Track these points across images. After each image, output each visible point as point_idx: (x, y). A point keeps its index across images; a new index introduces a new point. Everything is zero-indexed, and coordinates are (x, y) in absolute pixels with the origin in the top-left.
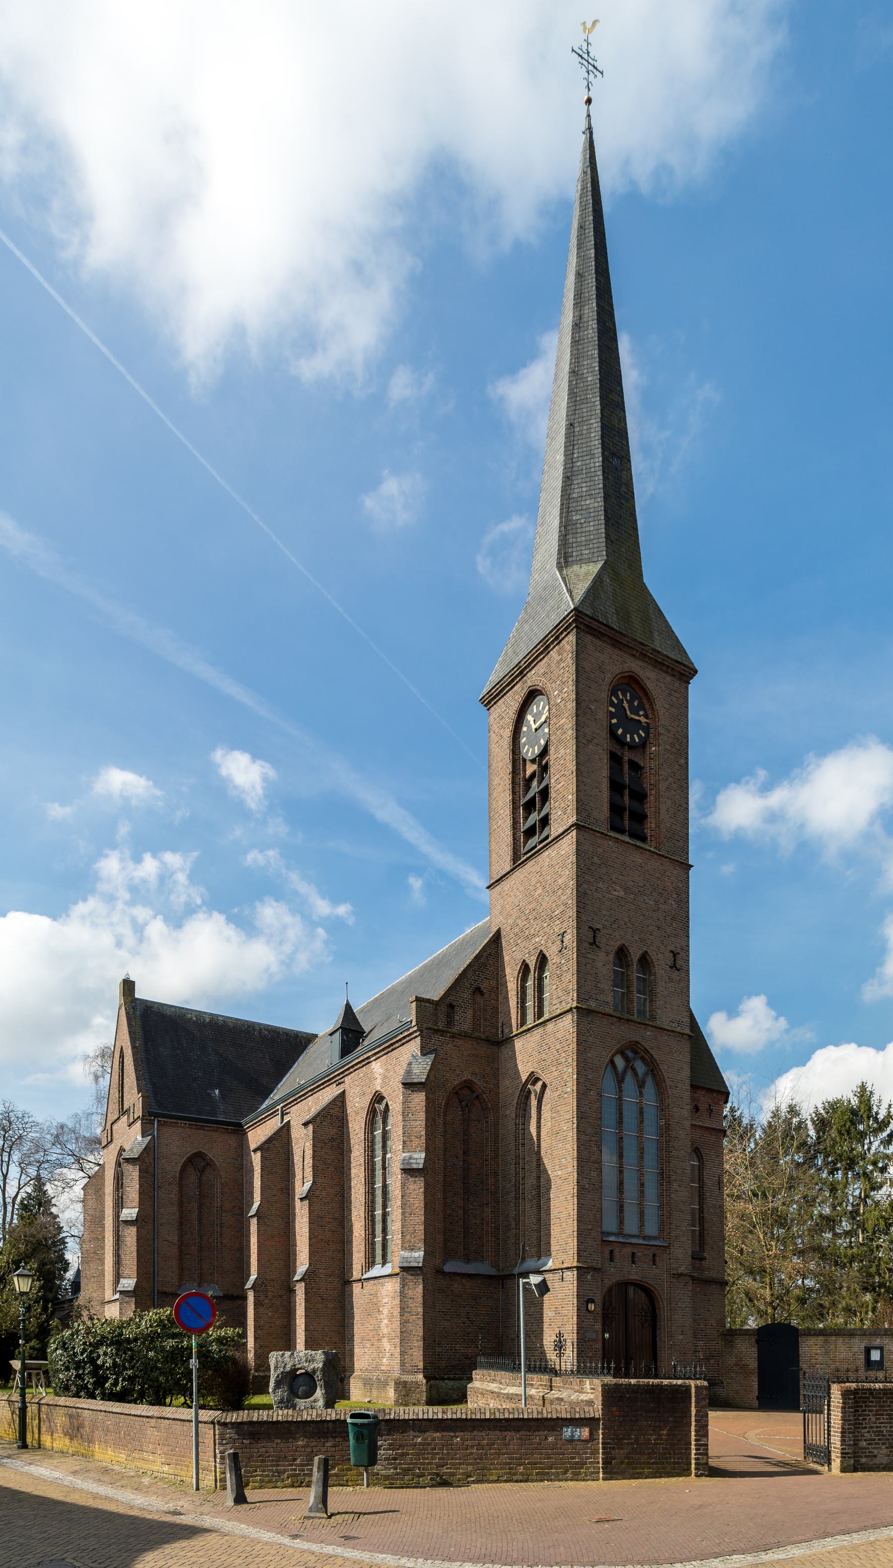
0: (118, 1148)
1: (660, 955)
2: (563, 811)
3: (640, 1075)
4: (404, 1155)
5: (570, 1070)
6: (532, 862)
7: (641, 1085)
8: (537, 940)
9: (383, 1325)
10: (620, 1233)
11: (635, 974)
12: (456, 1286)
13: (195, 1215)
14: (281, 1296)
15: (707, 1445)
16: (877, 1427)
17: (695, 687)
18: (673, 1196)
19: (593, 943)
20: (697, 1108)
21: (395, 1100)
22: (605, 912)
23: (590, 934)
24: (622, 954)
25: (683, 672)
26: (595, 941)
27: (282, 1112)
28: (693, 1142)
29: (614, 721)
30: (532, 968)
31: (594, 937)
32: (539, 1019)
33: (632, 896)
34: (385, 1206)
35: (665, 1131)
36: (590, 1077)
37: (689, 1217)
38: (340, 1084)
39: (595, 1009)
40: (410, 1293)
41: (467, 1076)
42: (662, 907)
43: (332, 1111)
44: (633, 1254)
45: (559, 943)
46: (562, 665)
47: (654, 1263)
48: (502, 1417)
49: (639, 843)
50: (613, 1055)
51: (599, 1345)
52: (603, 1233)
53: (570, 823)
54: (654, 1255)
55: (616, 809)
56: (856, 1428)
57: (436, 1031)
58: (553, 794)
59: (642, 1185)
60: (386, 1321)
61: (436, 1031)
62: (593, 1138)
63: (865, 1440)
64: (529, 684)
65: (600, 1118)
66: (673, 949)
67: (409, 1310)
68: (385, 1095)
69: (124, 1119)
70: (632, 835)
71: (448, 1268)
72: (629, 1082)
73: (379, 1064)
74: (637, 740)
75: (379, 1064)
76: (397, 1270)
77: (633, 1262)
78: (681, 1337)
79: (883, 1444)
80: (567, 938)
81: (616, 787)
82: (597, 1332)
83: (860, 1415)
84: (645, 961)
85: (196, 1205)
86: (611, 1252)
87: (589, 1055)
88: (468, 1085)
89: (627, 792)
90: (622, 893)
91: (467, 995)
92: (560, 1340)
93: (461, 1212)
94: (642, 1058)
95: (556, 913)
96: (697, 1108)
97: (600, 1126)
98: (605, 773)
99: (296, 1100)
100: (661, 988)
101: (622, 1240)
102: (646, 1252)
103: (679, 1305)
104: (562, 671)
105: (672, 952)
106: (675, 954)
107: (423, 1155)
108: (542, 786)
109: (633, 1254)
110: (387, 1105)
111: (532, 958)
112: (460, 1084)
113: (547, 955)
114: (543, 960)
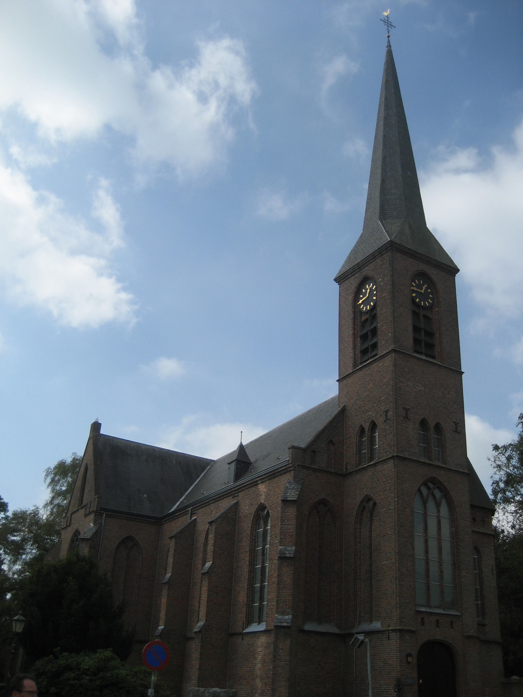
0: (74, 530)
2: (385, 343)
4: (281, 547)
5: (393, 495)
6: (367, 368)
7: (438, 505)
8: (370, 413)
10: (428, 606)
19: (406, 417)
20: (474, 520)
21: (275, 511)
24: (424, 423)
26: (407, 416)
27: (191, 512)
29: (414, 295)
30: (366, 430)
31: (407, 413)
32: (371, 461)
34: (262, 581)
35: (455, 536)
38: (235, 496)
39: (408, 457)
44: (437, 621)
45: (384, 416)
46: (384, 266)
50: (420, 486)
52: (416, 605)
53: (390, 348)
54: (452, 622)
55: (417, 341)
57: (304, 467)
58: (379, 332)
60: (259, 665)
64: (364, 274)
65: (413, 526)
68: (267, 506)
69: (82, 511)
70: (426, 355)
71: (309, 627)
73: (264, 486)
75: (264, 486)
76: (273, 628)
77: (438, 627)
80: (390, 413)
81: (416, 329)
84: (438, 428)
86: (422, 619)
88: (323, 502)
89: (423, 332)
90: (422, 388)
94: (438, 488)
95: (382, 399)
98: (410, 322)
99: (202, 505)
101: (429, 610)
104: (384, 269)
105: (454, 422)
106: (456, 424)
107: (294, 548)
109: (437, 621)
110: (268, 512)
113: (377, 423)
114: (374, 426)
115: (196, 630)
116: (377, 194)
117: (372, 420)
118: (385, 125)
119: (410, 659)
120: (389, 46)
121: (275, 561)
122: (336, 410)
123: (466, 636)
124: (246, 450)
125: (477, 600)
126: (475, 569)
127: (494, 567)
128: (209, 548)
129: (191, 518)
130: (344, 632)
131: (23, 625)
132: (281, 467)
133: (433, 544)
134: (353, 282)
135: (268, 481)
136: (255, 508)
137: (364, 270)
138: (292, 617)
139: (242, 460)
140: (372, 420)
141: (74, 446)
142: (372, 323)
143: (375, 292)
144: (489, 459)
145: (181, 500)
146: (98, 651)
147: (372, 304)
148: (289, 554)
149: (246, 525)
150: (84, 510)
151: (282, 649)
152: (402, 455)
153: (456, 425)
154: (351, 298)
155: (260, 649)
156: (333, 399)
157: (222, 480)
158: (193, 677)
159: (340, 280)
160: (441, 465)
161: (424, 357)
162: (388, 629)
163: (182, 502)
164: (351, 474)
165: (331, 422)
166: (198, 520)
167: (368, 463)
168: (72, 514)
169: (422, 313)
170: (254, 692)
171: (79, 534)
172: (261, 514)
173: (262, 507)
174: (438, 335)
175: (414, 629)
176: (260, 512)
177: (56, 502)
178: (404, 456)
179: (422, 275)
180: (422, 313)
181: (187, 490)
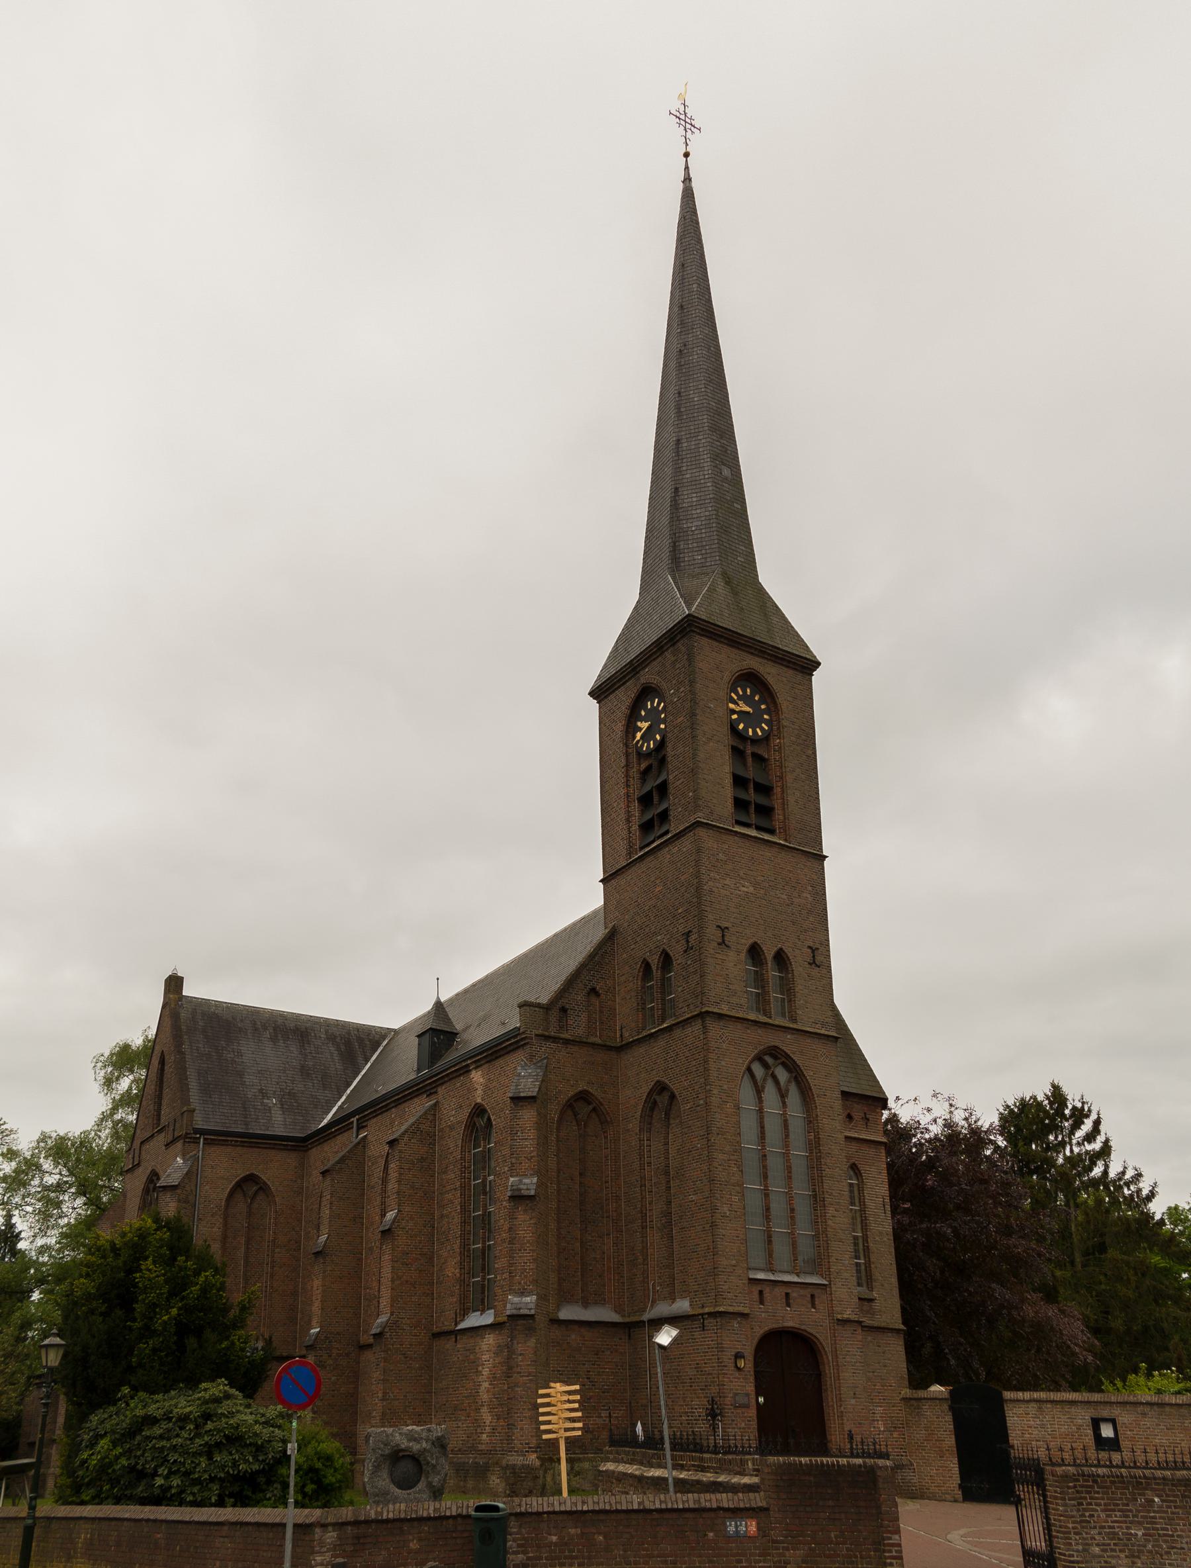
0: (149, 1172)
1: (797, 952)
3: (782, 1083)
7: (783, 1095)
9: (482, 1388)
11: (772, 973)
12: (574, 1337)
13: (241, 1252)
14: (347, 1355)
16: (1110, 1527)
17: (817, 676)
18: (830, 1222)
19: (723, 942)
24: (755, 952)
28: (848, 1158)
29: (735, 717)
30: (654, 968)
32: (663, 1022)
33: (762, 892)
35: (815, 1146)
37: (851, 1248)
40: (519, 1348)
41: (583, 1086)
42: (796, 901)
43: (422, 1127)
44: (787, 1295)
47: (813, 1306)
49: (766, 837)
50: (751, 1062)
51: (753, 1412)
54: (813, 1296)
55: (740, 804)
56: (1083, 1527)
57: (547, 1038)
59: (792, 1210)
60: (486, 1385)
61: (547, 1038)
63: (1098, 1545)
64: (643, 681)
66: (811, 944)
69: (161, 1139)
70: (758, 828)
71: (565, 1314)
72: (770, 1093)
77: (788, 1305)
78: (853, 1401)
79: (1121, 1551)
81: (739, 781)
82: (747, 1395)
83: (1085, 1510)
84: (781, 959)
85: (243, 1241)
86: (761, 1292)
88: (583, 1097)
90: (751, 889)
91: (580, 997)
94: (783, 1064)
96: (850, 1117)
97: (739, 1143)
100: (800, 987)
102: (802, 1292)
105: (810, 947)
106: (813, 950)
107: (535, 1180)
108: (658, 782)
109: (787, 1295)
110: (489, 1119)
119: (741, 1363)
120: (687, 180)
122: (600, 933)
125: (857, 1257)
126: (853, 1204)
127: (887, 1200)
128: (390, 1187)
131: (61, 1352)
134: (624, 697)
139: (438, 1032)
141: (140, 1022)
142: (660, 772)
145: (339, 1103)
147: (658, 737)
149: (453, 1142)
152: (716, 1010)
154: (620, 727)
155: (485, 1357)
156: (595, 913)
157: (405, 1067)
158: (374, 1414)
159: (599, 693)
162: (701, 1311)
163: (340, 1107)
164: (629, 1045)
165: (591, 957)
168: (142, 1143)
171: (158, 1179)
172: (479, 1122)
177: (117, 1117)
179: (750, 678)
180: (749, 750)
181: (349, 1086)
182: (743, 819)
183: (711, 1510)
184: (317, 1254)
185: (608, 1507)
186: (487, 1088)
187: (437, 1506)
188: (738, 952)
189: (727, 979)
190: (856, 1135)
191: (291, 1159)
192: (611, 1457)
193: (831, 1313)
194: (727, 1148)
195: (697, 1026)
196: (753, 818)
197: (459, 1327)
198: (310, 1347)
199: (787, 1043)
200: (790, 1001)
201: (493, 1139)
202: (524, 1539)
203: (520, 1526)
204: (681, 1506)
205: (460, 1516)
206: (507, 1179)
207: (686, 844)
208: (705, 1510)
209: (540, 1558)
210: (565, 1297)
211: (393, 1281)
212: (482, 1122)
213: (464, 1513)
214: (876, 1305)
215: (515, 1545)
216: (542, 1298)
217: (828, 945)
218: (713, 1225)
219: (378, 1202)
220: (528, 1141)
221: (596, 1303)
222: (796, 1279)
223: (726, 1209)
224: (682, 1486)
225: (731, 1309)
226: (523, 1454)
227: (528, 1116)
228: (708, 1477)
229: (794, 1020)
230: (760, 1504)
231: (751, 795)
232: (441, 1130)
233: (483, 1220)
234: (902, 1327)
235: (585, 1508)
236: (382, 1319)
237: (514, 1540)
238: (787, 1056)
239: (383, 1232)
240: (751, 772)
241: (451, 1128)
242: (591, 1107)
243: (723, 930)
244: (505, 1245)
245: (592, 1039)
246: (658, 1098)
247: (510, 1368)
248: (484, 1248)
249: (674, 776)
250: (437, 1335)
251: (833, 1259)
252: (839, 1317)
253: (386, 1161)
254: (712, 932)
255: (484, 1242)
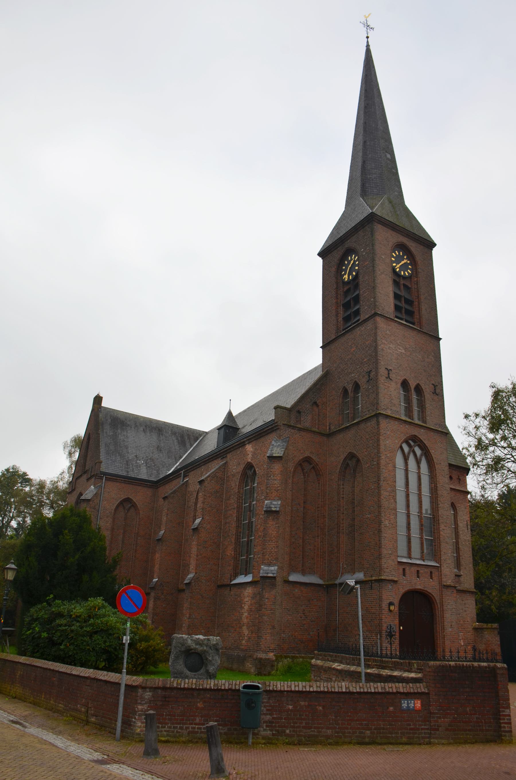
7: (418, 462)
9: (244, 616)
10: (410, 557)
11: (414, 397)
12: (297, 591)
15: (509, 715)
20: (451, 478)
22: (394, 361)
23: (386, 372)
24: (405, 384)
25: (429, 245)
26: (389, 376)
27: (184, 474)
30: (349, 391)
31: (389, 374)
32: (354, 420)
36: (388, 455)
38: (223, 458)
39: (391, 415)
41: (307, 454)
44: (418, 571)
45: (367, 376)
46: (366, 237)
47: (431, 578)
48: (355, 691)
50: (402, 443)
54: (431, 572)
55: (397, 308)
57: (290, 426)
58: (361, 298)
62: (391, 494)
66: (433, 382)
67: (265, 607)
69: (85, 477)
70: (406, 321)
71: (293, 578)
72: (412, 462)
74: (407, 274)
75: (251, 446)
77: (418, 577)
78: (450, 630)
81: (397, 297)
84: (418, 389)
87: (387, 442)
88: (308, 460)
90: (403, 351)
92: (390, 631)
93: (301, 541)
95: (365, 360)
97: (395, 486)
99: (193, 467)
101: (410, 561)
102: (426, 570)
103: (449, 607)
105: (433, 384)
106: (435, 386)
107: (279, 502)
109: (418, 571)
110: (255, 471)
111: (350, 385)
112: (303, 459)
115: (186, 582)
116: (359, 174)
117: (355, 381)
118: (365, 113)
119: (392, 608)
121: (261, 516)
122: (320, 373)
123: (444, 586)
124: (236, 420)
129: (183, 481)
130: (327, 583)
132: (267, 427)
133: (414, 499)
134: (337, 255)
135: (255, 441)
136: (242, 466)
137: (346, 243)
138: (278, 569)
139: (229, 427)
140: (355, 381)
143: (357, 263)
144: (459, 427)
146: (89, 599)
147: (354, 273)
148: (275, 507)
149: (234, 483)
150: (86, 475)
151: (267, 598)
152: (384, 413)
153: (435, 387)
154: (334, 269)
155: (246, 600)
157: (210, 445)
158: (184, 625)
160: (421, 424)
161: (405, 323)
162: (370, 579)
166: (189, 481)
167: (351, 422)
169: (402, 282)
170: (241, 638)
172: (249, 471)
173: (249, 466)
174: (417, 303)
175: (396, 579)
176: (247, 471)
178: (387, 414)
179: (401, 247)
180: (402, 282)
182: (399, 315)
183: (393, 693)
184: (159, 540)
185: (326, 690)
186: (254, 454)
187: (216, 682)
188: (396, 383)
189: (391, 397)
190: (454, 487)
191: (149, 492)
192: (321, 657)
193: (440, 581)
194: (389, 489)
195: (374, 422)
196: (404, 316)
197: (232, 583)
198: (153, 588)
199: (421, 434)
200: (423, 412)
201: (256, 482)
202: (271, 706)
203: (269, 698)
204: (373, 691)
205: (230, 689)
206: (264, 502)
207: (369, 325)
208: (389, 693)
209: (281, 718)
210: (293, 569)
211: (197, 556)
212: (250, 473)
213: (233, 688)
214: (462, 579)
215: (265, 709)
216: (281, 568)
217: (442, 384)
218: (380, 531)
219: (192, 515)
220: (276, 481)
221: (310, 573)
222: (422, 563)
223: (387, 522)
224: (370, 678)
225: (387, 578)
226: (266, 652)
227: (277, 467)
228: (386, 672)
229: (425, 422)
230: (423, 690)
231: (403, 304)
232: (228, 477)
233: (248, 526)
234: (475, 590)
235: (311, 690)
236: (191, 576)
237: (265, 707)
238: (421, 441)
239: (193, 529)
240: (403, 293)
241: (234, 476)
242: (312, 466)
243: (389, 371)
244: (261, 539)
245: (313, 429)
246: (350, 462)
247: (261, 606)
248: (248, 541)
249: (363, 292)
250: (220, 586)
251: (442, 553)
252: (445, 584)
253: (197, 494)
254: (382, 371)
255: (248, 538)
